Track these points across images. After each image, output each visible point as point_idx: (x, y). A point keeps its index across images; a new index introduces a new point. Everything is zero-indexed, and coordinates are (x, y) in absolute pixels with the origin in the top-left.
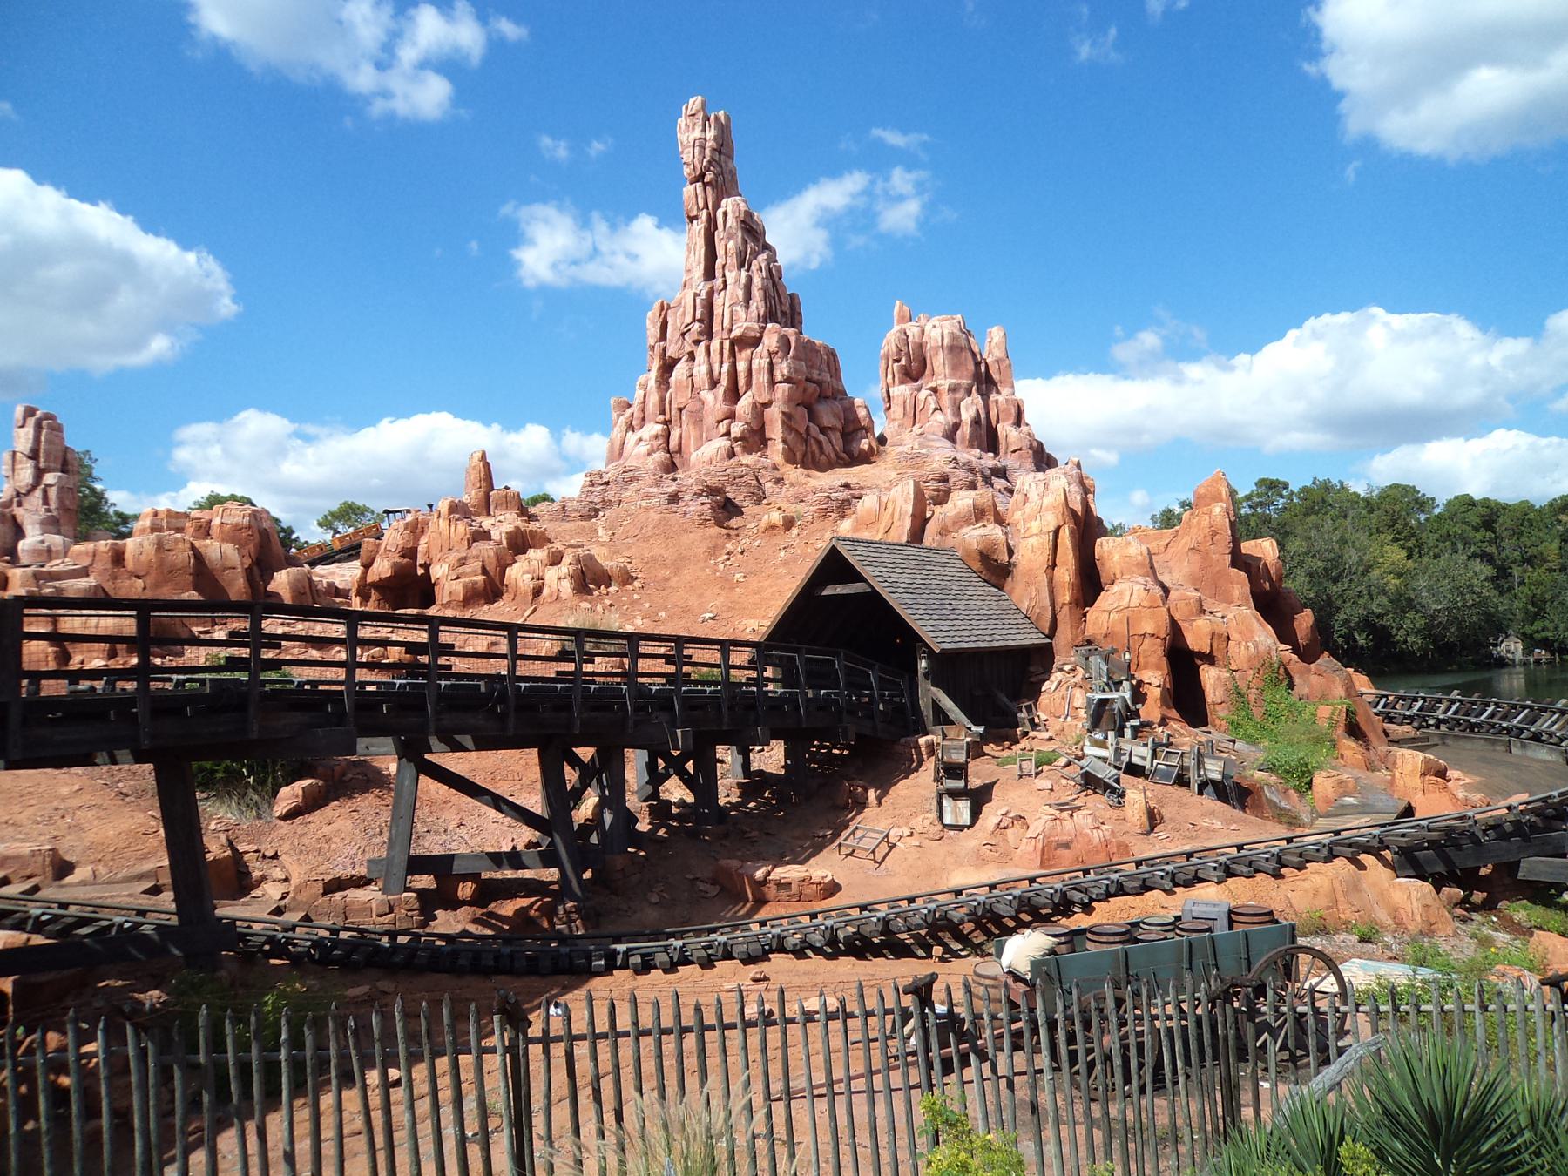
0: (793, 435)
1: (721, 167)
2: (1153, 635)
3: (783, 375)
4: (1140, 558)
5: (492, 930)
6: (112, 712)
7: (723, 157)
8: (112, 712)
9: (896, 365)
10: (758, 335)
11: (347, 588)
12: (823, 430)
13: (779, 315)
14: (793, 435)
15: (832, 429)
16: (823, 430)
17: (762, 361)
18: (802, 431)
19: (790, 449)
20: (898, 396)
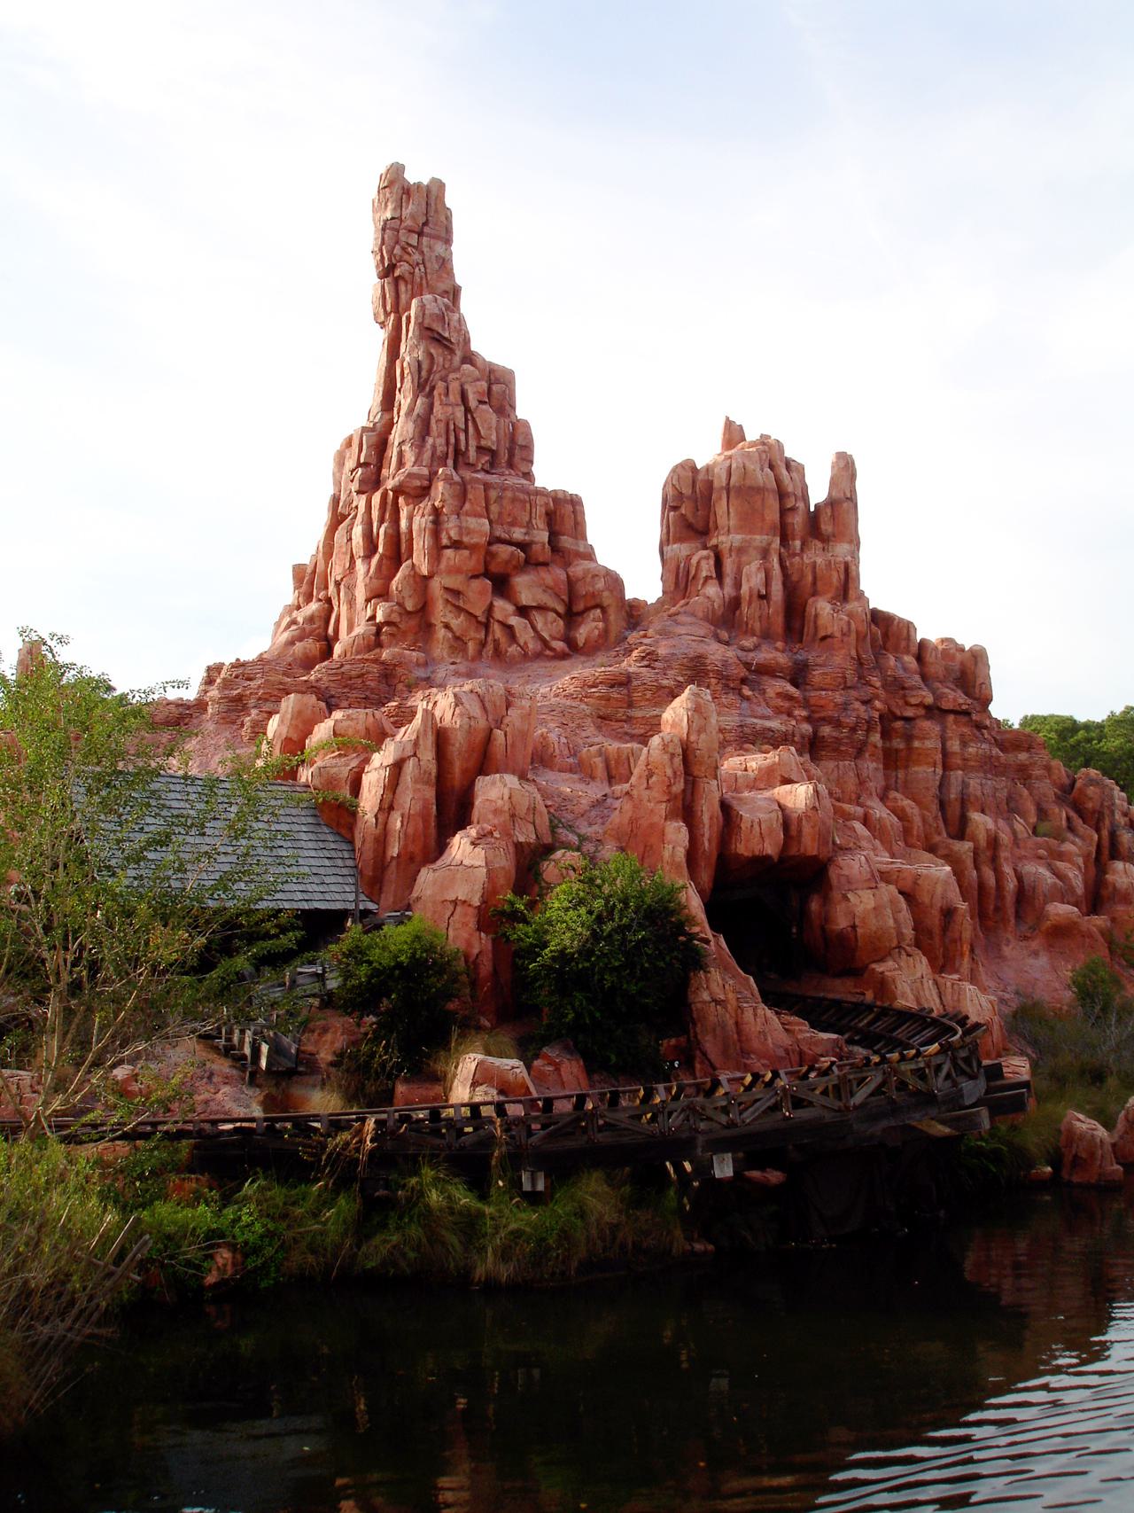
0: (462, 617)
1: (422, 253)
2: (465, 902)
3: (450, 538)
4: (500, 803)
5: (836, 1481)
6: (668, 1164)
7: (425, 240)
8: (668, 1164)
9: (672, 513)
10: (426, 483)
11: (512, 849)
12: (523, 611)
13: (472, 453)
14: (462, 617)
15: (541, 608)
16: (523, 611)
17: (424, 520)
18: (479, 612)
19: (457, 638)
20: (671, 558)
